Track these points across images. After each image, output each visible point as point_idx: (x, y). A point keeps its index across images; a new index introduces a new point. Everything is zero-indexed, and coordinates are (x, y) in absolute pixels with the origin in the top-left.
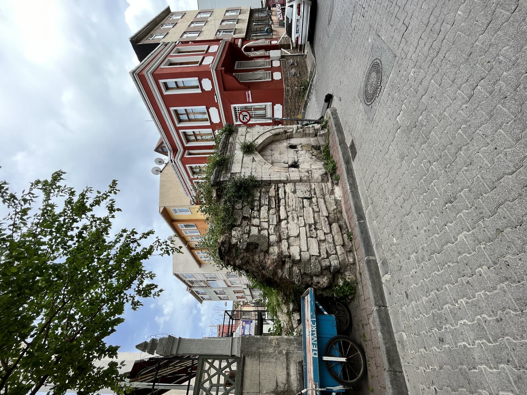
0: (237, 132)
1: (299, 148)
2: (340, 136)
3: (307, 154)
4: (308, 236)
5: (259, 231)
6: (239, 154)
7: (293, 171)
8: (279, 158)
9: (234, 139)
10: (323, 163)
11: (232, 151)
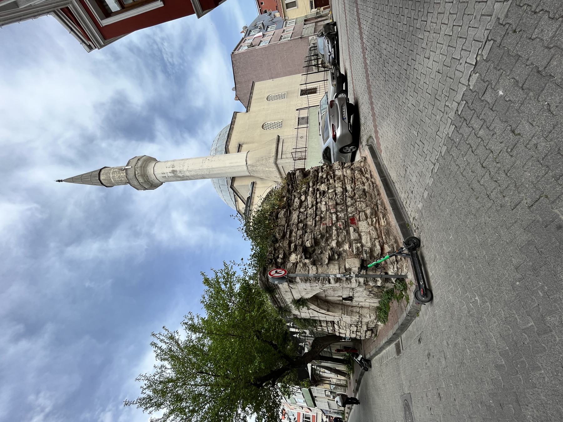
3: (365, 292)
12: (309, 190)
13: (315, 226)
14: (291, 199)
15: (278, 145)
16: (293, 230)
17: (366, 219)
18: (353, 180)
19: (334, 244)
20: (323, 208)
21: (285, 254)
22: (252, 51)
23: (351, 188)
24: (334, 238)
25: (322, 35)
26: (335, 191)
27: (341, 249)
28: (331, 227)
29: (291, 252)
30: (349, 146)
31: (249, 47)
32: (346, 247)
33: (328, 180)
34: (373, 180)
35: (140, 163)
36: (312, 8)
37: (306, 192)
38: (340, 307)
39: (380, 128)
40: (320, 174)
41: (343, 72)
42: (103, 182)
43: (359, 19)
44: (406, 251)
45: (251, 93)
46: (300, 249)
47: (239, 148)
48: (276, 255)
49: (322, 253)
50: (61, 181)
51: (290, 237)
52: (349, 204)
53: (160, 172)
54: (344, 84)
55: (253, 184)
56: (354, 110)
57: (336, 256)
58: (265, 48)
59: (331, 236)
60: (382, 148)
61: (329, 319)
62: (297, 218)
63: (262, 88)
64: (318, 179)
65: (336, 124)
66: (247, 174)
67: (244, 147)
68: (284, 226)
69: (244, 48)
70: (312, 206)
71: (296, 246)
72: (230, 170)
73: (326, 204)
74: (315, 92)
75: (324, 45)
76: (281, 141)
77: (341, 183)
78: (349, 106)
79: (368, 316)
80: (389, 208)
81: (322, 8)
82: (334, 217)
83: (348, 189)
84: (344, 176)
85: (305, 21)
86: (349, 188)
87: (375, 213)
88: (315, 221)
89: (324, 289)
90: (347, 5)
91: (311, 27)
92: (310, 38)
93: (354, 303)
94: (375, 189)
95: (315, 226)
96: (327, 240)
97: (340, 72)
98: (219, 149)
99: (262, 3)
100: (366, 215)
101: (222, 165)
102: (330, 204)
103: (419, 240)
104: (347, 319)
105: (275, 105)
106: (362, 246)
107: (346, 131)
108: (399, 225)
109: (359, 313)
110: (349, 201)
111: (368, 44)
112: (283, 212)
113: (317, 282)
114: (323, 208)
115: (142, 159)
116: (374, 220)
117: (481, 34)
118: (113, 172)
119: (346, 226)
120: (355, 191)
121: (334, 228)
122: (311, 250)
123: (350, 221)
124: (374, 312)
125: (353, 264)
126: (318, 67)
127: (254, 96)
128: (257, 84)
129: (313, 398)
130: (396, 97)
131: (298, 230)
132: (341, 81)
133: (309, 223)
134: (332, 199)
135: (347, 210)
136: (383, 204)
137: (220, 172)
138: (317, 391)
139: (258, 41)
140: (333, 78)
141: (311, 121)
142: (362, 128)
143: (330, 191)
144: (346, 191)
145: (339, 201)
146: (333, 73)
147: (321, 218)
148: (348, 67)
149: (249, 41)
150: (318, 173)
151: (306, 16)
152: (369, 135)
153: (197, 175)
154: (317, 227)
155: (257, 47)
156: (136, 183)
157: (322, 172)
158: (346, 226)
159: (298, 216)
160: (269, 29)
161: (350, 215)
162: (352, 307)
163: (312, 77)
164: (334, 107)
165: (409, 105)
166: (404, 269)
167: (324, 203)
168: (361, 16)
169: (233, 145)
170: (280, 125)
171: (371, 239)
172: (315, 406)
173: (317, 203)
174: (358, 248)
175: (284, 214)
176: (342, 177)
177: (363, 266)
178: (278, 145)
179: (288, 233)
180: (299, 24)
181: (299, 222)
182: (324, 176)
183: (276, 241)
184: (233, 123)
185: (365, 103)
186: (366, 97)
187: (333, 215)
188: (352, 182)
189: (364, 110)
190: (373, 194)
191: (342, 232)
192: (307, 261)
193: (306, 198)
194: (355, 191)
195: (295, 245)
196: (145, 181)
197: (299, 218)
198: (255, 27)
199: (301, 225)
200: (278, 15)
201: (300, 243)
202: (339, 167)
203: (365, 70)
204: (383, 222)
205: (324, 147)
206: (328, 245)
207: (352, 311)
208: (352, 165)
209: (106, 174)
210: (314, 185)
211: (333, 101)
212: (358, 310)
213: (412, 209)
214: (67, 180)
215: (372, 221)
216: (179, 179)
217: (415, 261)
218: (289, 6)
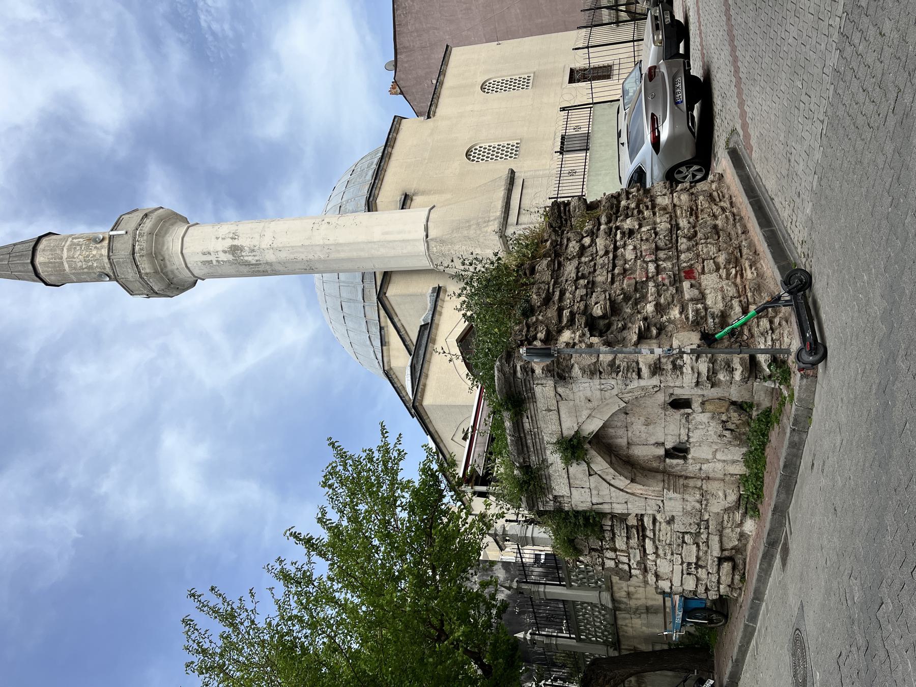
0: (533, 398)
1: (696, 405)
2: (783, 496)
3: (713, 424)
4: (685, 572)
5: (617, 565)
6: (555, 459)
7: (670, 499)
8: (644, 435)
9: (534, 420)
10: (744, 450)
11: (540, 451)
12: (599, 229)
13: (613, 282)
14: (561, 245)
16: (566, 290)
18: (693, 211)
19: (650, 308)
20: (629, 254)
23: (689, 223)
24: (650, 299)
26: (655, 229)
27: (664, 318)
28: (645, 283)
29: (563, 328)
32: (675, 313)
34: (735, 210)
37: (593, 233)
39: (749, 103)
40: (623, 203)
41: (679, 17)
42: (40, 269)
44: (786, 297)
45: (442, 73)
46: (580, 320)
47: (406, 201)
48: (532, 334)
54: (682, 45)
56: (700, 91)
59: (644, 297)
60: (753, 142)
61: (635, 508)
62: (574, 271)
63: (470, 63)
64: (618, 211)
65: (659, 115)
66: (425, 264)
67: (417, 200)
68: (548, 284)
70: (607, 253)
71: (572, 314)
72: (383, 251)
73: (635, 248)
74: (608, 77)
76: (518, 183)
77: (668, 216)
78: (691, 81)
79: (721, 494)
82: (652, 268)
83: (681, 225)
84: (675, 206)
86: (683, 223)
87: (735, 260)
88: (613, 275)
89: (627, 397)
93: (692, 468)
94: (738, 224)
95: (613, 282)
97: (672, 16)
98: (350, 207)
101: (362, 238)
102: (644, 247)
103: (809, 276)
106: (706, 309)
108: (779, 268)
109: (701, 488)
110: (683, 244)
113: (614, 375)
114: (629, 254)
115: (154, 216)
116: (733, 271)
118: (72, 244)
119: (676, 281)
120: (697, 229)
121: (651, 284)
122: (602, 323)
123: (683, 274)
124: (734, 487)
125: (689, 340)
126: (618, 10)
127: (450, 80)
130: (772, 34)
131: (576, 288)
133: (600, 279)
134: (647, 240)
135: (678, 258)
136: (751, 245)
137: (354, 254)
140: (656, 28)
141: (594, 144)
142: (717, 121)
143: (643, 229)
144: (678, 229)
145: (661, 244)
146: (656, 18)
147: (625, 270)
150: (619, 202)
152: (730, 129)
153: (295, 261)
154: (616, 284)
156: (130, 274)
157: (628, 198)
158: (676, 281)
159: (577, 268)
161: (685, 265)
162: (686, 478)
164: (658, 78)
165: (791, 40)
166: (785, 339)
167: (631, 247)
169: (389, 191)
170: (514, 151)
171: (723, 298)
173: (616, 248)
174: (697, 311)
175: (548, 266)
176: (670, 207)
177: (708, 339)
179: (557, 293)
181: (578, 278)
182: (633, 205)
183: (529, 311)
184: (390, 142)
185: (723, 67)
187: (650, 264)
188: (691, 215)
190: (733, 233)
191: (668, 289)
192: (595, 340)
193: (593, 242)
194: (697, 229)
195: (571, 312)
196: (156, 272)
197: (578, 272)
199: (582, 282)
201: (582, 307)
202: (665, 191)
203: (723, 8)
204: (749, 274)
206: (639, 312)
207: (685, 486)
208: (691, 187)
211: (655, 67)
212: (699, 483)
215: (728, 274)
216: (245, 269)
217: (803, 316)
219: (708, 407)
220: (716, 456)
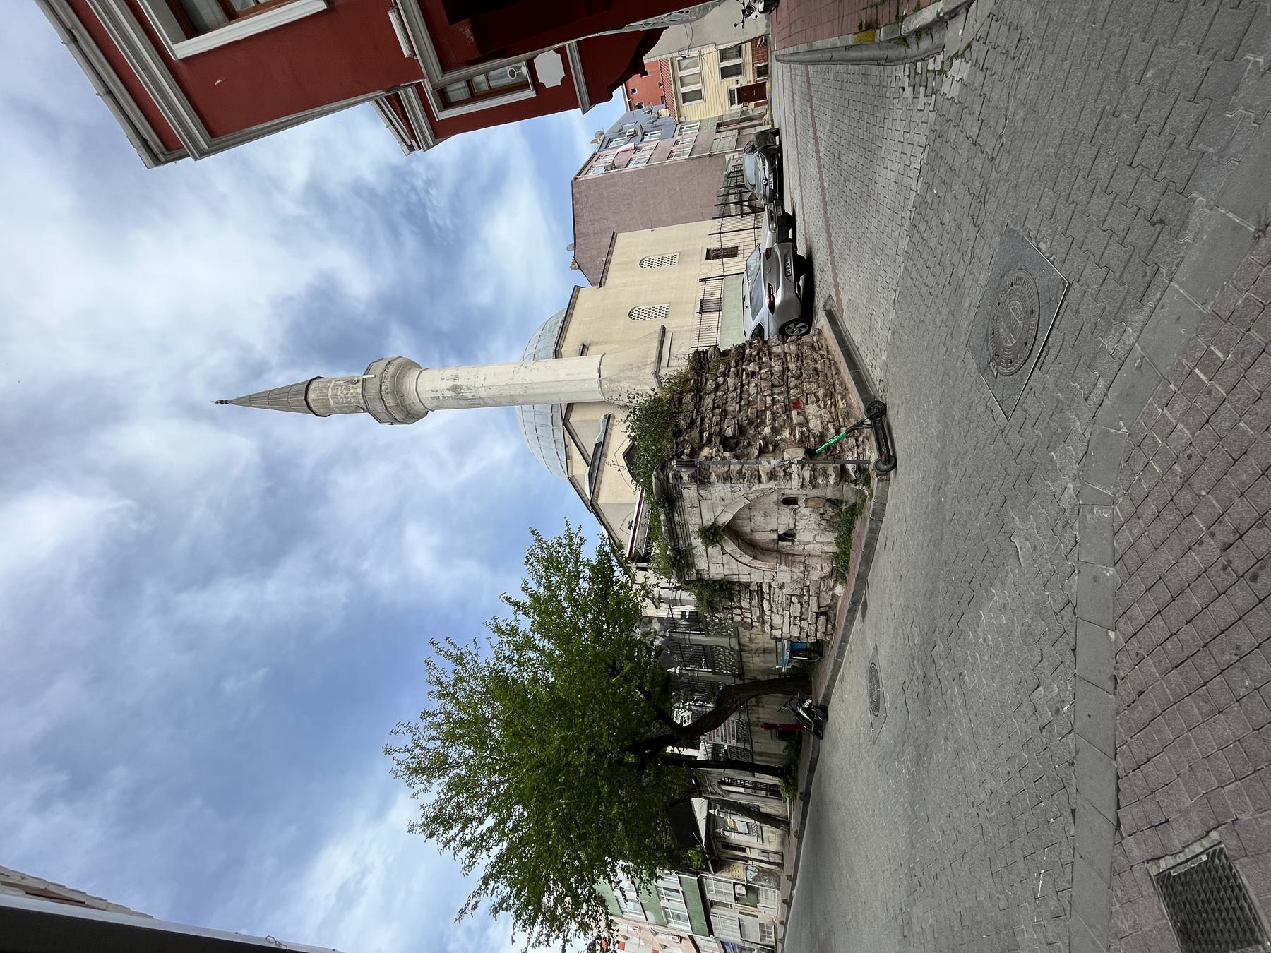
1: (801, 502)
6: (697, 542)
9: (682, 515)
11: (687, 537)
13: (740, 411)
15: (662, 342)
17: (817, 401)
18: (800, 358)
19: (768, 430)
20: (752, 390)
21: (692, 449)
22: (613, 177)
25: (753, 150)
30: (795, 322)
31: (607, 168)
32: (786, 434)
33: (760, 358)
35: (391, 369)
36: (732, 103)
38: (774, 555)
40: (747, 351)
41: (788, 211)
42: (312, 404)
43: (814, 125)
45: (610, 252)
46: (716, 440)
47: (584, 350)
49: (749, 445)
50: (226, 402)
51: (702, 424)
52: (792, 385)
53: (429, 388)
55: (609, 417)
56: (805, 266)
57: (770, 447)
58: (637, 173)
59: (763, 422)
61: (756, 577)
65: (774, 285)
66: (599, 397)
69: (597, 171)
70: (735, 389)
72: (566, 388)
74: (735, 255)
75: (755, 168)
76: (668, 336)
78: (797, 259)
80: (851, 384)
81: (752, 104)
82: (769, 400)
85: (719, 125)
86: (792, 366)
87: (830, 394)
90: (797, 103)
91: (729, 137)
92: (728, 157)
93: (798, 548)
95: (740, 411)
96: (757, 427)
99: (633, 91)
100: (817, 397)
104: (785, 574)
105: (652, 275)
106: (809, 431)
107: (792, 295)
111: (826, 160)
112: (689, 396)
114: (752, 390)
115: (395, 363)
117: (921, 139)
119: (787, 410)
122: (732, 441)
127: (615, 259)
128: (621, 238)
129: (707, 906)
132: (785, 224)
133: (730, 409)
136: (842, 383)
137: (546, 391)
138: (719, 885)
139: (625, 158)
140: (771, 219)
142: (817, 289)
145: (776, 382)
148: (797, 200)
149: (607, 158)
151: (721, 117)
155: (624, 170)
156: (379, 407)
158: (787, 410)
160: (646, 139)
163: (730, 223)
164: (773, 257)
168: (817, 120)
169: (571, 343)
170: (665, 312)
172: (711, 932)
173: (742, 386)
174: (802, 432)
177: (810, 453)
178: (662, 342)
180: (705, 130)
181: (714, 408)
183: (677, 433)
184: (571, 306)
186: (824, 238)
189: (820, 260)
192: (727, 454)
193: (725, 380)
198: (621, 133)
199: (718, 411)
200: (664, 112)
204: (841, 405)
205: (751, 326)
209: (321, 390)
210: (737, 365)
213: (875, 364)
214: (240, 402)
216: (463, 403)
218: (687, 98)
219: (810, 503)
220: (815, 538)
